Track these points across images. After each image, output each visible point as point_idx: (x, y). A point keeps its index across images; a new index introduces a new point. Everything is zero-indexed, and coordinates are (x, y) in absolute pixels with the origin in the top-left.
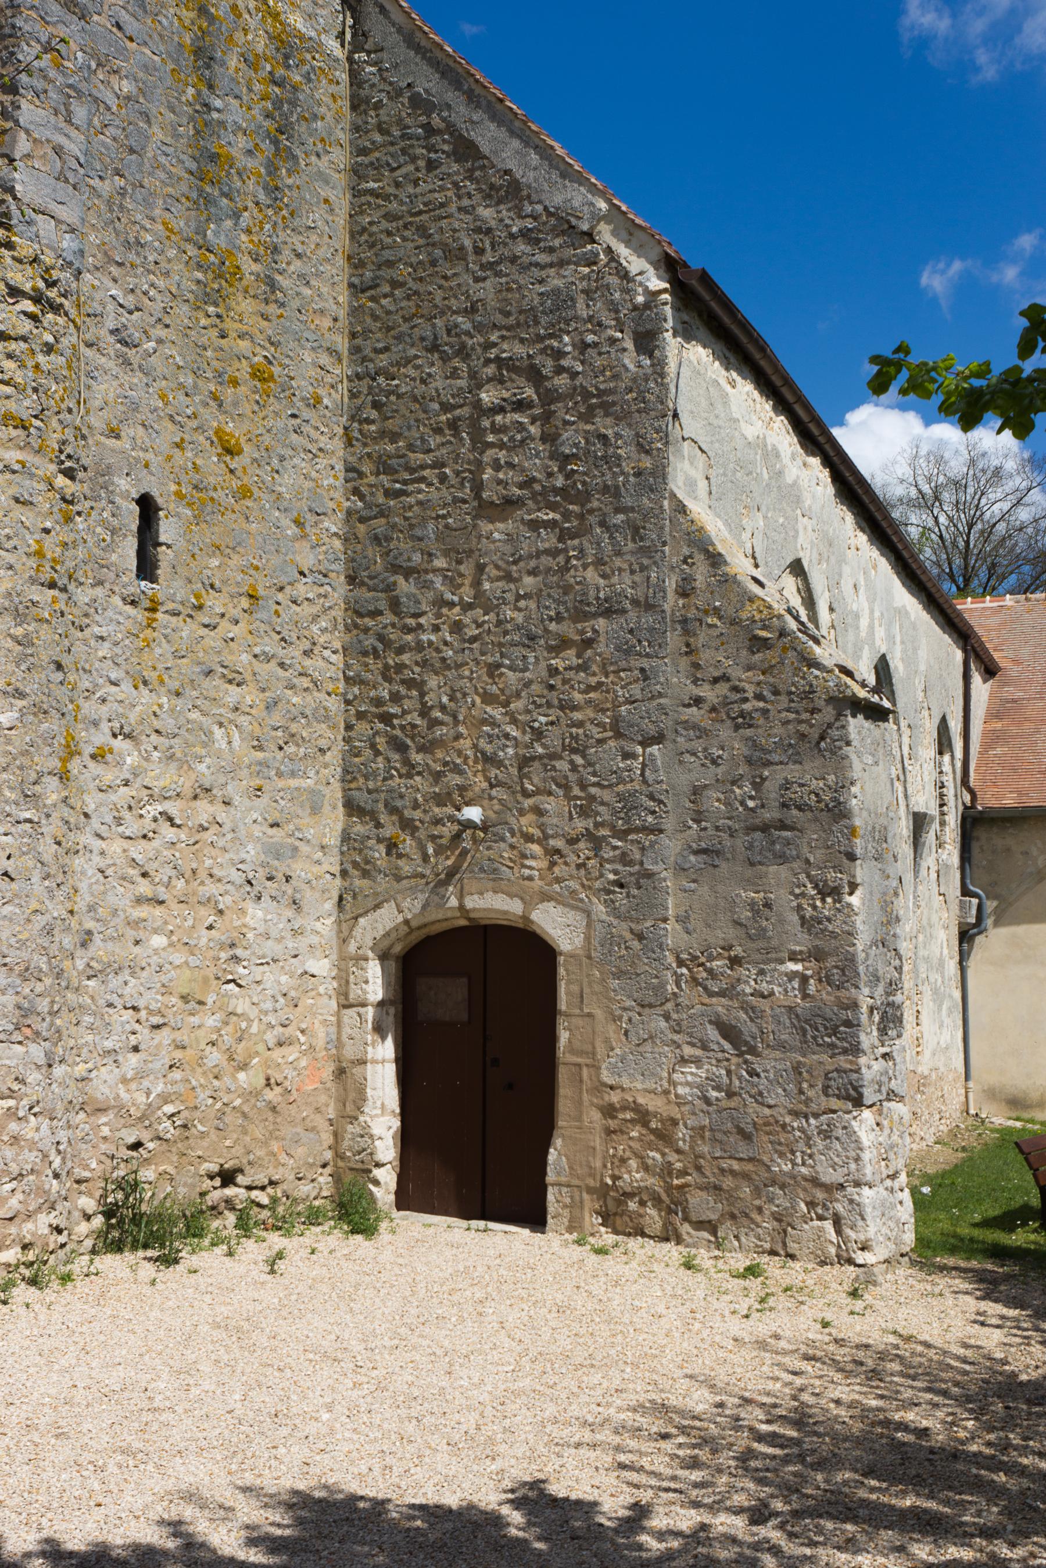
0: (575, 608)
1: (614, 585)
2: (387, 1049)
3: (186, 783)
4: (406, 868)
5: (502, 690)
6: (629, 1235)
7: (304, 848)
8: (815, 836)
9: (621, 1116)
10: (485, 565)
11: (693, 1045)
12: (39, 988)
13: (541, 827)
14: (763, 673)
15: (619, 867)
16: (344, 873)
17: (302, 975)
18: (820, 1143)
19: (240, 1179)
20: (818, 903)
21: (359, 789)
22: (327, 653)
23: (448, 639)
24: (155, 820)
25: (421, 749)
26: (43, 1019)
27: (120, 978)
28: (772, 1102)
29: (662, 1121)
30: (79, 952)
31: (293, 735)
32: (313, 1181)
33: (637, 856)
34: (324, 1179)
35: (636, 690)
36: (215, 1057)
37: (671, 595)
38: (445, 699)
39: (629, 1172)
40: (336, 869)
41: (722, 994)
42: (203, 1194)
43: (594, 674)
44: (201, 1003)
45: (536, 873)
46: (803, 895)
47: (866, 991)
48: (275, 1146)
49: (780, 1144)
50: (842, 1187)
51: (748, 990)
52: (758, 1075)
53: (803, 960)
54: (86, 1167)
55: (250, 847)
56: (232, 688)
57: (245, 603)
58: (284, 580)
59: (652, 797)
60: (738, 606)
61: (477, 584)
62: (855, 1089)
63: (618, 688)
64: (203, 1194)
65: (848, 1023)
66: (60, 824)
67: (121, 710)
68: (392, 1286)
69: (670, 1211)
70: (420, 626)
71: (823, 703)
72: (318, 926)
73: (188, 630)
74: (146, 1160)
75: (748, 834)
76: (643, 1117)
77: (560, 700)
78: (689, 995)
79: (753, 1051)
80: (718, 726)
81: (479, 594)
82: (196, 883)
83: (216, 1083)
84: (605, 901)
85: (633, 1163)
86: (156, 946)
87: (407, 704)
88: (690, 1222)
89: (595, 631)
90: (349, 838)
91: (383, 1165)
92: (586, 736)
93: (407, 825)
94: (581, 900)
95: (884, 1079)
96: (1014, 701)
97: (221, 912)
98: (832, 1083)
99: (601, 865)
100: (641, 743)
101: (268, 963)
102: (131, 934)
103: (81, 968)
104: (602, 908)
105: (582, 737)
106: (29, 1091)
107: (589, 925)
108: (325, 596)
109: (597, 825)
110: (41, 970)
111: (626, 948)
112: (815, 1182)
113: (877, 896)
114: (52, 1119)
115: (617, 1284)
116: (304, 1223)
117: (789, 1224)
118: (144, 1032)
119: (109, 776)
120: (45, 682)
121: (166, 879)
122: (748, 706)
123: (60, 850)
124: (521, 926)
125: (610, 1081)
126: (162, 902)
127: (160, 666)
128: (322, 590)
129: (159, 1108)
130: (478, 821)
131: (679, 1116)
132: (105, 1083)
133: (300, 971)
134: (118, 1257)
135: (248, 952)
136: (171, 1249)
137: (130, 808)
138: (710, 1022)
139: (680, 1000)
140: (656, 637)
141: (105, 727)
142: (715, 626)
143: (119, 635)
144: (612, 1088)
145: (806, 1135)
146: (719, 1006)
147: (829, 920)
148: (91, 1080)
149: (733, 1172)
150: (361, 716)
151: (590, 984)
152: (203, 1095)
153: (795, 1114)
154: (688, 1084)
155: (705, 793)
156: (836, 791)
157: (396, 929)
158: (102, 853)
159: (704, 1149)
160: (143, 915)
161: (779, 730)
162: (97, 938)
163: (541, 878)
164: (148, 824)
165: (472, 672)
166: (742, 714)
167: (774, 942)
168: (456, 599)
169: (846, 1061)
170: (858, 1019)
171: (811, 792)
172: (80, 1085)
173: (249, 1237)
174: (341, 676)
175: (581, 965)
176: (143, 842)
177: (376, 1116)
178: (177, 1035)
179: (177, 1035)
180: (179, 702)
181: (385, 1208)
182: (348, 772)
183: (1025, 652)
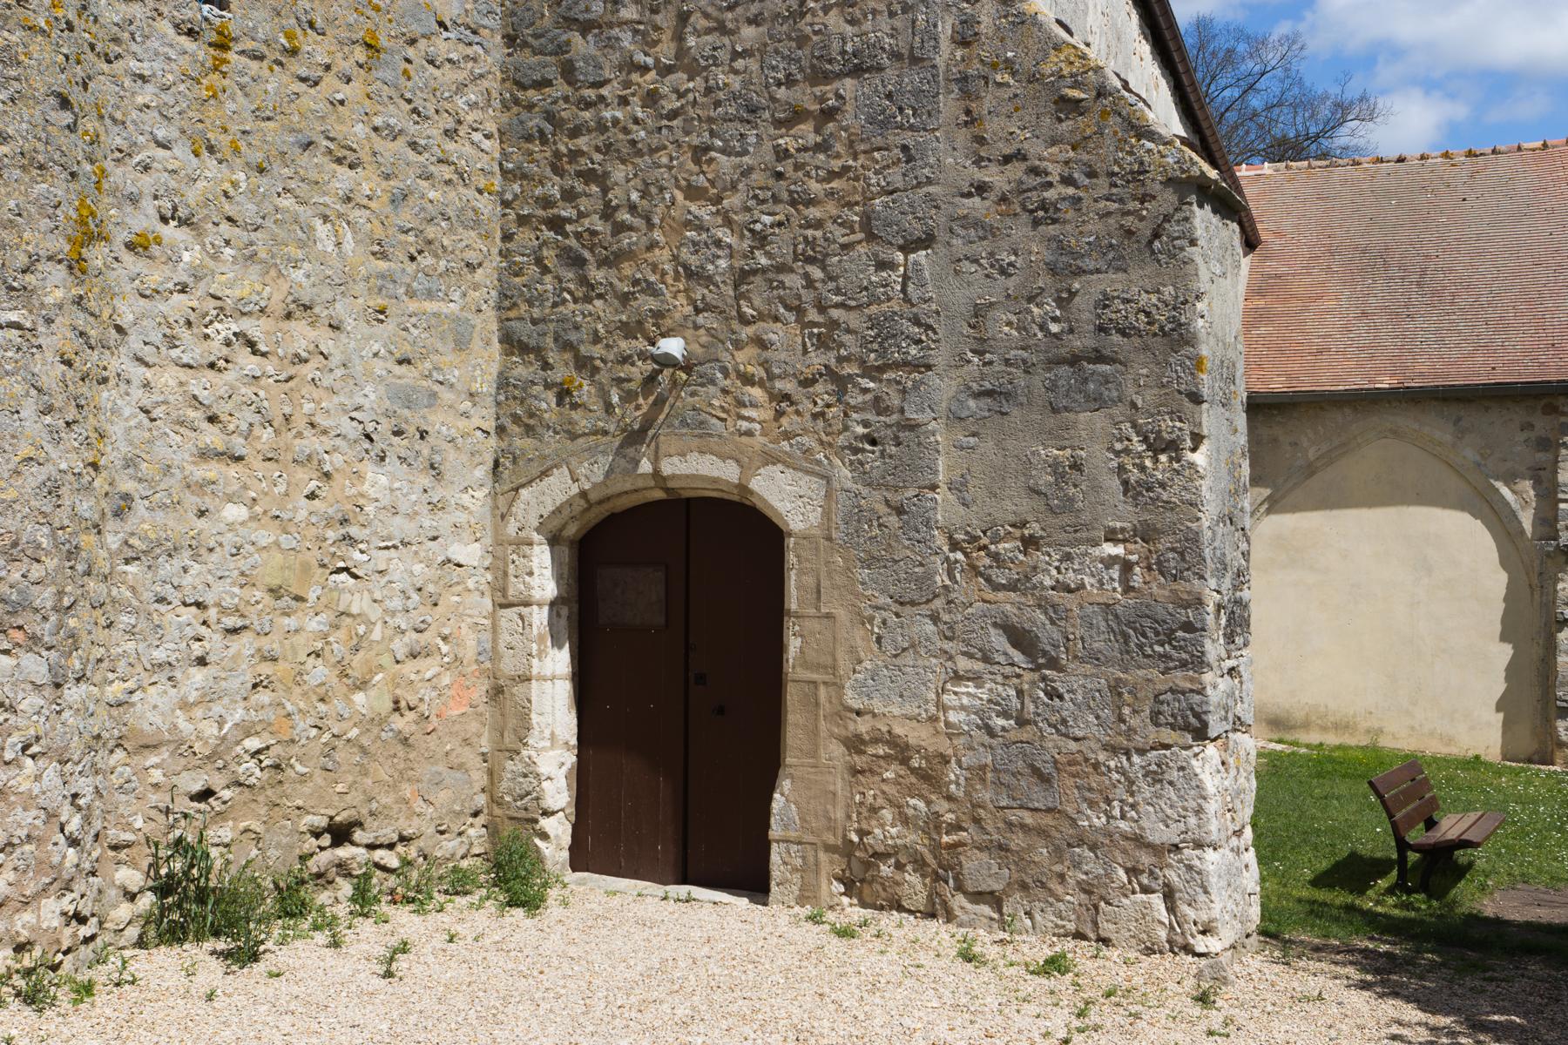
0: (813, 66)
1: (866, 34)
2: (560, 661)
3: (276, 296)
4: (583, 422)
5: (712, 183)
6: (882, 908)
7: (446, 395)
8: (1145, 371)
9: (871, 750)
10: (689, 13)
11: (971, 656)
12: (37, 572)
13: (765, 364)
14: (1074, 149)
15: (871, 416)
16: (501, 430)
17: (443, 563)
18: (1147, 791)
19: (358, 835)
20: (1148, 463)
21: (521, 319)
22: (477, 137)
23: (640, 115)
24: (228, 344)
25: (603, 263)
26: (45, 618)
27: (177, 563)
28: (1080, 734)
29: (926, 758)
30: (111, 525)
31: (430, 242)
32: (460, 834)
33: (896, 401)
34: (476, 832)
35: (895, 176)
36: (319, 672)
37: (945, 45)
38: (635, 196)
39: (882, 826)
40: (490, 425)
41: (1012, 587)
42: (303, 858)
43: (838, 156)
44: (298, 599)
45: (758, 426)
46: (1127, 451)
47: (1212, 583)
48: (407, 790)
49: (1090, 789)
50: (1176, 848)
51: (1048, 582)
52: (1061, 697)
53: (1124, 541)
54: (128, 827)
55: (368, 389)
56: (342, 171)
57: (360, 54)
58: (416, 29)
59: (916, 322)
60: (1040, 56)
61: (679, 38)
62: (1197, 716)
63: (871, 174)
64: (303, 858)
65: (1188, 627)
66: (70, 335)
67: (172, 184)
68: (558, 997)
69: (937, 878)
70: (602, 98)
71: (1158, 187)
72: (465, 499)
73: (276, 83)
74: (219, 814)
75: (1049, 370)
76: (901, 752)
77: (791, 192)
78: (966, 589)
79: (1054, 663)
80: (1009, 222)
81: (681, 52)
82: (290, 435)
83: (322, 707)
84: (851, 463)
85: (887, 814)
86: (230, 519)
87: (584, 204)
88: (965, 893)
89: (839, 97)
90: (508, 384)
91: (553, 813)
92: (826, 240)
93: (584, 364)
94: (819, 462)
95: (1231, 702)
96: (1277, 276)
97: (327, 475)
98: (1165, 707)
99: (846, 415)
100: (901, 248)
101: (395, 547)
102: (192, 501)
103: (114, 547)
104: (846, 472)
105: (821, 242)
106: (22, 722)
107: (828, 496)
108: (475, 60)
109: (840, 360)
110: (39, 546)
111: (880, 525)
112: (1139, 840)
113: (1224, 455)
114: (63, 762)
115: (874, 988)
116: (446, 892)
117: (1102, 898)
118: (214, 642)
119: (156, 276)
120: (40, 121)
121: (244, 426)
122: (1050, 194)
123: (70, 373)
124: (736, 498)
125: (856, 704)
126: (240, 459)
127: (234, 128)
128: (469, 51)
129: (238, 743)
130: (679, 357)
131: (950, 752)
132: (155, 708)
133: (440, 559)
134: (176, 949)
135: (367, 531)
136: (248, 940)
137: (189, 323)
138: (995, 625)
139: (953, 595)
140: (924, 101)
141: (149, 206)
142: (1007, 85)
143: (170, 77)
144: (858, 713)
145: (1127, 778)
146: (1008, 604)
147: (1163, 485)
148: (133, 705)
149: (1023, 826)
150: (523, 220)
151: (829, 573)
152: (302, 725)
153: (1113, 749)
154: (963, 708)
155: (990, 315)
156: (1174, 309)
157: (569, 503)
158: (146, 385)
159: (986, 795)
160: (211, 475)
161: (1095, 226)
162: (140, 506)
163: (764, 434)
164: (216, 348)
165: (671, 159)
166: (1043, 206)
167: (1085, 517)
168: (650, 61)
169: (1185, 678)
170: (1203, 621)
171: (1140, 311)
172: (115, 712)
173: (366, 916)
174: (496, 169)
175: (817, 549)
176: (210, 374)
177: (543, 749)
178: (265, 643)
179: (265, 643)
180: (264, 182)
181: (556, 870)
182: (506, 296)
183: (1287, 225)
